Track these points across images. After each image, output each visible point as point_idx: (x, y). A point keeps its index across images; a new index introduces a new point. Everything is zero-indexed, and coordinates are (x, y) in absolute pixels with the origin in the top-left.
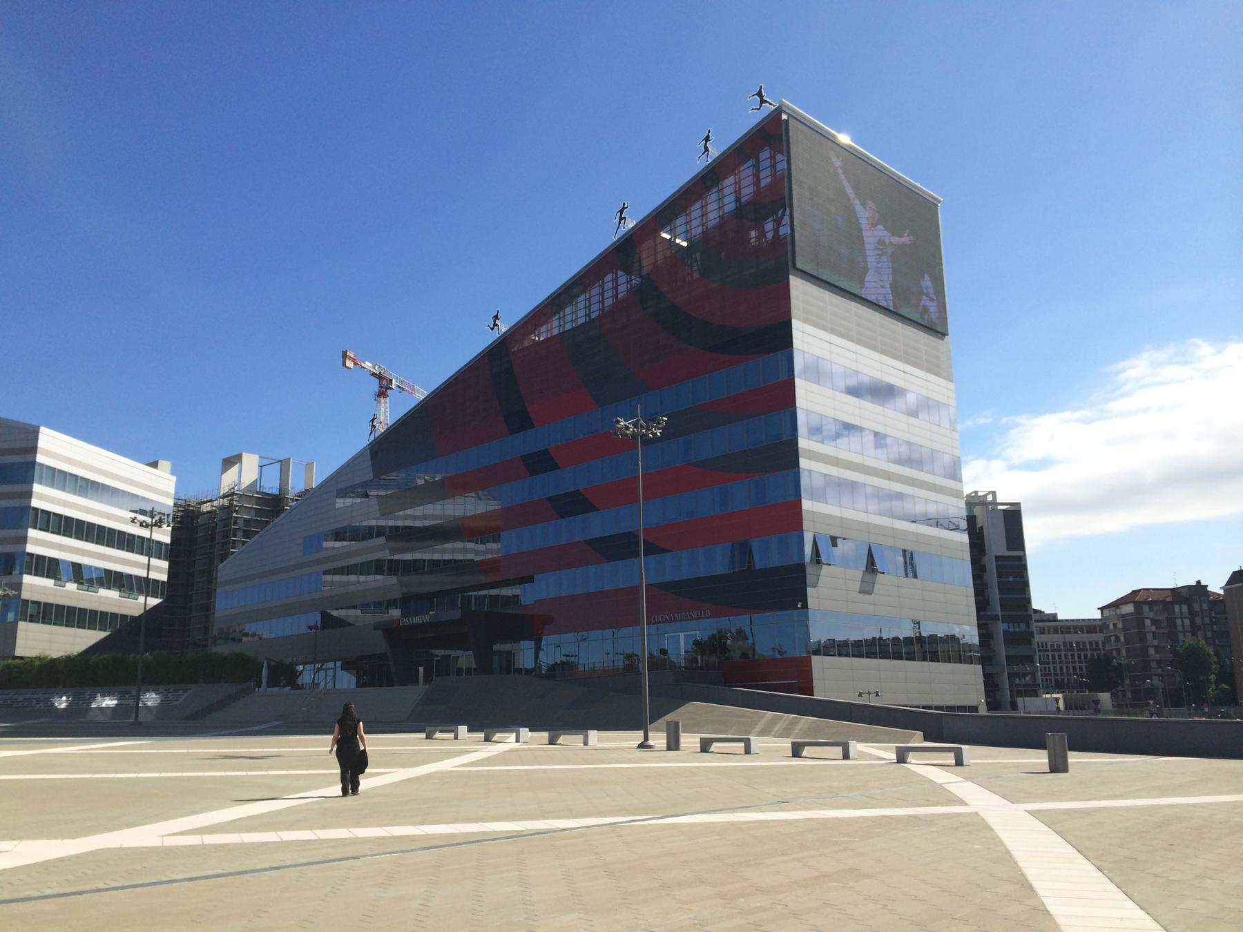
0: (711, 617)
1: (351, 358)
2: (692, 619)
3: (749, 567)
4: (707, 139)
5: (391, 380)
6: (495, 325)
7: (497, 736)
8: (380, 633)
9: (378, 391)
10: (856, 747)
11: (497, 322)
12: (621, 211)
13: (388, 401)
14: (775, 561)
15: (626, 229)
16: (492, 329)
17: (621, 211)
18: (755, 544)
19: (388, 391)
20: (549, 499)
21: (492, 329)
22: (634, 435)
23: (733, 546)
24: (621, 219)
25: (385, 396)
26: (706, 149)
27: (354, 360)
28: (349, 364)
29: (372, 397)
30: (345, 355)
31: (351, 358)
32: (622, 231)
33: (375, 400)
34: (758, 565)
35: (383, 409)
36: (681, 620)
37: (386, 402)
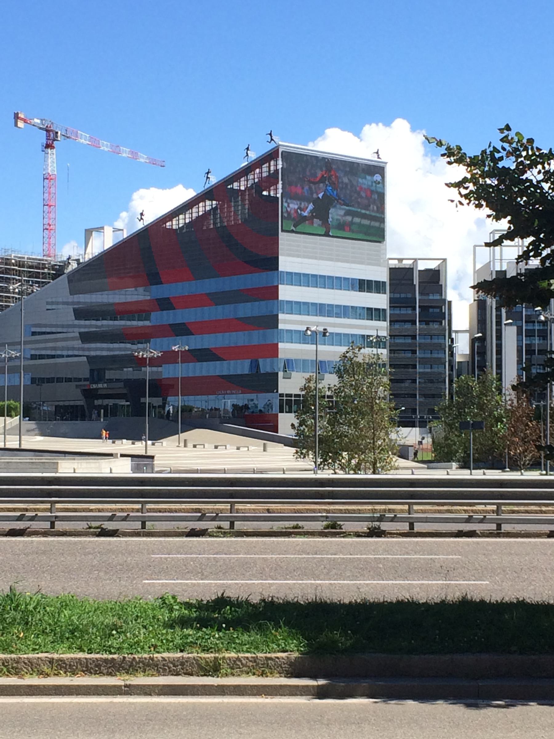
0: (241, 393)
1: (22, 119)
2: (233, 394)
3: (257, 372)
4: (248, 149)
5: (57, 133)
6: (142, 219)
7: (136, 443)
8: (79, 391)
9: (45, 143)
10: (251, 448)
11: (143, 217)
12: (208, 173)
13: (55, 152)
14: (269, 370)
15: (209, 185)
16: (140, 220)
17: (208, 173)
18: (261, 361)
19: (55, 142)
20: (174, 309)
21: (140, 220)
22: (178, 351)
23: (251, 361)
24: (207, 178)
25: (52, 147)
26: (247, 155)
27: (25, 121)
28: (21, 124)
29: (40, 148)
30: (16, 117)
31: (22, 119)
32: (207, 186)
33: (43, 151)
34: (262, 372)
35: (50, 161)
36: (229, 394)
37: (53, 154)
